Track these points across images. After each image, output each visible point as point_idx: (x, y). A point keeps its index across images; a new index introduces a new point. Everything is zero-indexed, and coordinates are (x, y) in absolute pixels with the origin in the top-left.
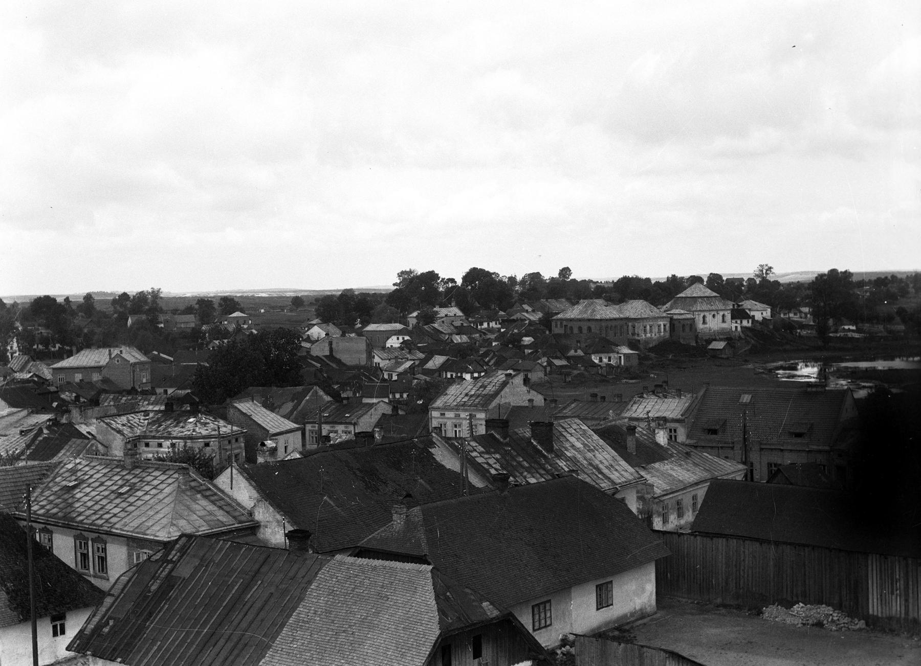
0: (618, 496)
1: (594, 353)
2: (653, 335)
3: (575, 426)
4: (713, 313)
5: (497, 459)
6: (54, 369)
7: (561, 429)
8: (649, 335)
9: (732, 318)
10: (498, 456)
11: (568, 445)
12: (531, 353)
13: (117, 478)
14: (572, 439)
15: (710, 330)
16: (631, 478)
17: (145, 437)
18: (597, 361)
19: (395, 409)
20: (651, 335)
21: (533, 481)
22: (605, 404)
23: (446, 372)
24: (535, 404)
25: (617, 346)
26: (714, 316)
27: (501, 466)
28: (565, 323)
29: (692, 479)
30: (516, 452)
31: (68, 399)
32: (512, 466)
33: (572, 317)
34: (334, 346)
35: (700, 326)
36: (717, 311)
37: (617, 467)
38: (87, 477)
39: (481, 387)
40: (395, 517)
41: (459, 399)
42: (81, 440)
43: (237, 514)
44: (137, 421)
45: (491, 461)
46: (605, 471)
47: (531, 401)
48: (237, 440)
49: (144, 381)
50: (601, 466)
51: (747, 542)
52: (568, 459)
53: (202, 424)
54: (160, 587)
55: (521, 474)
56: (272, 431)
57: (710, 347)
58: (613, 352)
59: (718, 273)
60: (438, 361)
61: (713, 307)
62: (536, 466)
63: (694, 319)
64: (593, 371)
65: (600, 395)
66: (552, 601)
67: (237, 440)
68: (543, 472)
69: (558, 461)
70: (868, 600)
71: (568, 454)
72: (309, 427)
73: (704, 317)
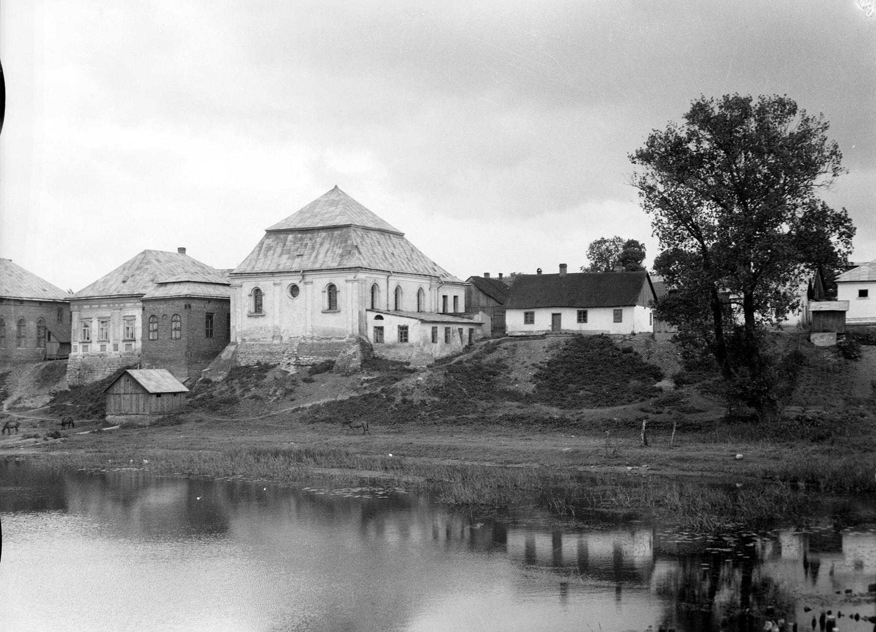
2: (109, 347)
20: (103, 347)
26: (294, 290)
29: (358, 518)
30: (739, 459)
59: (314, 199)
63: (226, 301)
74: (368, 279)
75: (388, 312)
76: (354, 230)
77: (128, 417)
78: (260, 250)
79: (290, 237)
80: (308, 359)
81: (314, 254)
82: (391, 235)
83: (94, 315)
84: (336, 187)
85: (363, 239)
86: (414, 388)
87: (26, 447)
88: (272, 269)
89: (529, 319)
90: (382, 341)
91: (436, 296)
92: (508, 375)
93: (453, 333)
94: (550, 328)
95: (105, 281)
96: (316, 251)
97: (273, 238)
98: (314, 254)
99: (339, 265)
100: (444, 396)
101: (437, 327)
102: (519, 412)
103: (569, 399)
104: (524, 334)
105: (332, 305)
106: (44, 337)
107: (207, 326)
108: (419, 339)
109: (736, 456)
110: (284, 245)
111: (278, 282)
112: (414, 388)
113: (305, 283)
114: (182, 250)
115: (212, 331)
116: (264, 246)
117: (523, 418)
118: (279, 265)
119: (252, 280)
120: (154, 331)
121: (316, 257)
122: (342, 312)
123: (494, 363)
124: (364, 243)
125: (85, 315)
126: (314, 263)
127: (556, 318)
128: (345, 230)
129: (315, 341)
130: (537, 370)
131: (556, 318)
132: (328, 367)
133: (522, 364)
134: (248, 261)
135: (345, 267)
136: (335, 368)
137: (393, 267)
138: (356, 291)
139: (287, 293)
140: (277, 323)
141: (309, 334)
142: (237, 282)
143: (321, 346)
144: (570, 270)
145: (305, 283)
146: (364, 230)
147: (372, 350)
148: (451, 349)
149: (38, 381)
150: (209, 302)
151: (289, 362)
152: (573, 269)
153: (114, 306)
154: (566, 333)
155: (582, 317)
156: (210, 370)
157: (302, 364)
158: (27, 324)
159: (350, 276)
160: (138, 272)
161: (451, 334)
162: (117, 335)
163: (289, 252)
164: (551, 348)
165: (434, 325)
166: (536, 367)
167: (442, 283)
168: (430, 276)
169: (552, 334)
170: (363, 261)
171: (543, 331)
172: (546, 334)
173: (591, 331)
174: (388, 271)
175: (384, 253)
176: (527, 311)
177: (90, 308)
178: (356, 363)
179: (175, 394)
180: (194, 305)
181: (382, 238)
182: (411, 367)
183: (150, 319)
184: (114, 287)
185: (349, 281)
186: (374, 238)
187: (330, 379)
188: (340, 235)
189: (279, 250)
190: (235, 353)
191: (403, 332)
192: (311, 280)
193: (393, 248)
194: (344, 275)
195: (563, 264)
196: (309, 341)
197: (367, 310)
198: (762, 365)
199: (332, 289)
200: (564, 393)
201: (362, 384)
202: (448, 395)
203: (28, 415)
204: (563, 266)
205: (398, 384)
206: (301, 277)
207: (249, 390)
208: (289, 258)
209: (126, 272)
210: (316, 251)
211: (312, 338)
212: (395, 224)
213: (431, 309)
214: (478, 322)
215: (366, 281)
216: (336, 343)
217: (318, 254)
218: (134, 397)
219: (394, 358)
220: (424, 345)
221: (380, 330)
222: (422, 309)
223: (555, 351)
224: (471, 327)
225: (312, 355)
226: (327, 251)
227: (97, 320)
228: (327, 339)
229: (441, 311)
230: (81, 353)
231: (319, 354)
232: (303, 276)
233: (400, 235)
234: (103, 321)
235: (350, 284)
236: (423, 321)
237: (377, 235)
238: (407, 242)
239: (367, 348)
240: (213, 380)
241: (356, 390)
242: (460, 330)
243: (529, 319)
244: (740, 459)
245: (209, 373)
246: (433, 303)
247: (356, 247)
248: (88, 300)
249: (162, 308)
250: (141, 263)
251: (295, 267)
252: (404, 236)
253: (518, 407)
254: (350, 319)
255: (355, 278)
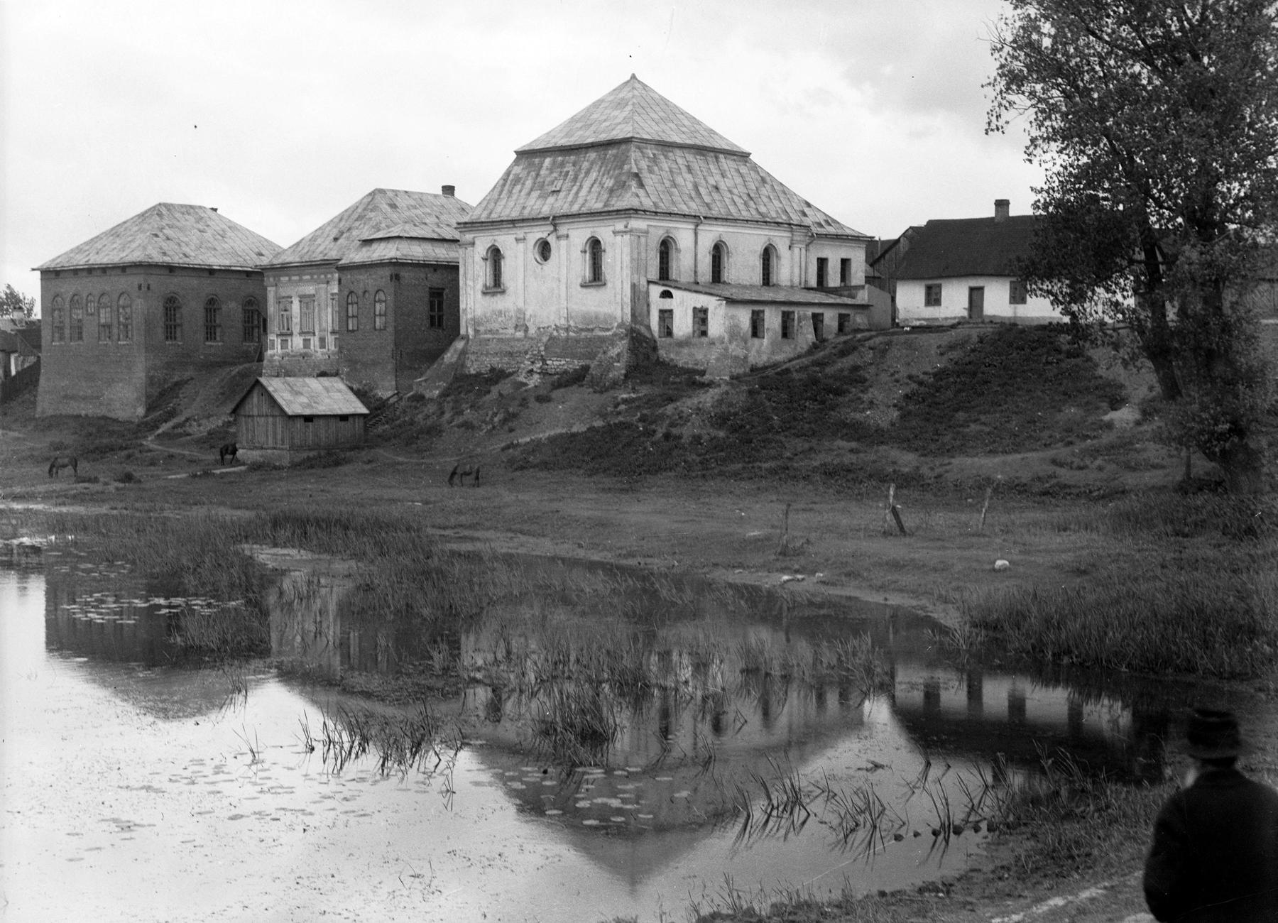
2: (315, 341)
26: (544, 249)
30: (999, 570)
40: (1175, 318)
63: (453, 269)
74: (651, 230)
75: (695, 287)
76: (639, 148)
77: (263, 452)
78: (504, 185)
79: (548, 161)
80: (557, 363)
81: (575, 189)
82: (721, 156)
83: (295, 290)
84: (634, 77)
85: (655, 162)
86: (691, 414)
87: (46, 497)
88: (515, 215)
89: (933, 298)
90: (704, 333)
91: (803, 259)
92: (862, 395)
93: (799, 321)
94: (965, 314)
95: (313, 238)
96: (578, 184)
97: (524, 163)
98: (575, 189)
99: (605, 206)
100: (734, 430)
101: (763, 311)
102: (848, 459)
103: (947, 438)
104: (924, 323)
105: (596, 278)
106: (259, 327)
107: (432, 309)
108: (722, 330)
109: (994, 563)
110: (538, 175)
111: (521, 236)
112: (691, 414)
113: (558, 238)
114: (449, 190)
115: (440, 318)
116: (511, 177)
117: (849, 471)
118: (524, 208)
119: (488, 233)
120: (353, 316)
121: (577, 193)
122: (609, 285)
123: (846, 373)
124: (656, 168)
125: (284, 292)
126: (572, 203)
127: (976, 296)
128: (623, 147)
129: (572, 334)
130: (914, 386)
131: (976, 296)
132: (577, 378)
133: (892, 375)
134: (485, 203)
135: (611, 209)
136: (588, 378)
137: (710, 209)
138: (627, 250)
139: (534, 254)
140: (521, 305)
141: (563, 322)
142: (468, 237)
143: (577, 341)
144: (1014, 211)
145: (558, 238)
146: (660, 148)
147: (655, 349)
148: (795, 348)
149: (223, 394)
150: (435, 270)
151: (530, 368)
152: (1022, 207)
153: (319, 277)
154: (991, 322)
155: (1018, 297)
156: (426, 381)
157: (549, 371)
158: (224, 308)
159: (620, 225)
160: (357, 224)
161: (796, 322)
162: (324, 325)
163: (542, 187)
164: (951, 347)
165: (757, 308)
166: (915, 382)
167: (813, 236)
168: (790, 224)
169: (969, 323)
170: (643, 199)
171: (955, 318)
172: (959, 323)
173: (1032, 319)
174: (695, 216)
175: (696, 187)
176: (930, 282)
177: (290, 280)
178: (619, 369)
179: (344, 418)
180: (405, 274)
181: (697, 162)
182: (707, 378)
183: (347, 299)
184: (321, 249)
185: (619, 232)
186: (680, 161)
187: (575, 396)
188: (615, 156)
189: (529, 183)
190: (463, 352)
191: (701, 316)
192: (565, 232)
193: (718, 178)
194: (611, 222)
195: (1002, 201)
196: (563, 334)
197: (649, 282)
198: (1230, 383)
199: (595, 246)
200: (941, 427)
201: (617, 406)
202: (742, 427)
203: (183, 446)
204: (1002, 205)
205: (670, 409)
206: (551, 228)
207: (461, 413)
208: (540, 197)
209: (341, 225)
210: (578, 184)
211: (567, 330)
212: (733, 134)
213: (791, 281)
214: (863, 303)
215: (647, 232)
216: (599, 337)
217: (581, 187)
218: (270, 419)
219: (687, 363)
220: (730, 342)
221: (666, 315)
222: (775, 281)
223: (955, 355)
224: (843, 311)
225: (564, 357)
226: (592, 185)
227: (298, 299)
228: (588, 330)
229: (813, 282)
230: (280, 351)
231: (573, 356)
232: (555, 225)
233: (744, 157)
234: (306, 300)
235: (619, 238)
236: (731, 301)
237: (687, 155)
238: (755, 168)
239: (644, 345)
240: (427, 396)
241: (603, 416)
242: (817, 319)
243: (933, 298)
244: (1003, 570)
245: (423, 384)
246: (797, 271)
247: (637, 175)
248: (284, 269)
249: (365, 280)
250: (365, 209)
251: (546, 211)
252: (751, 157)
253: (852, 451)
254: (619, 297)
255: (626, 227)
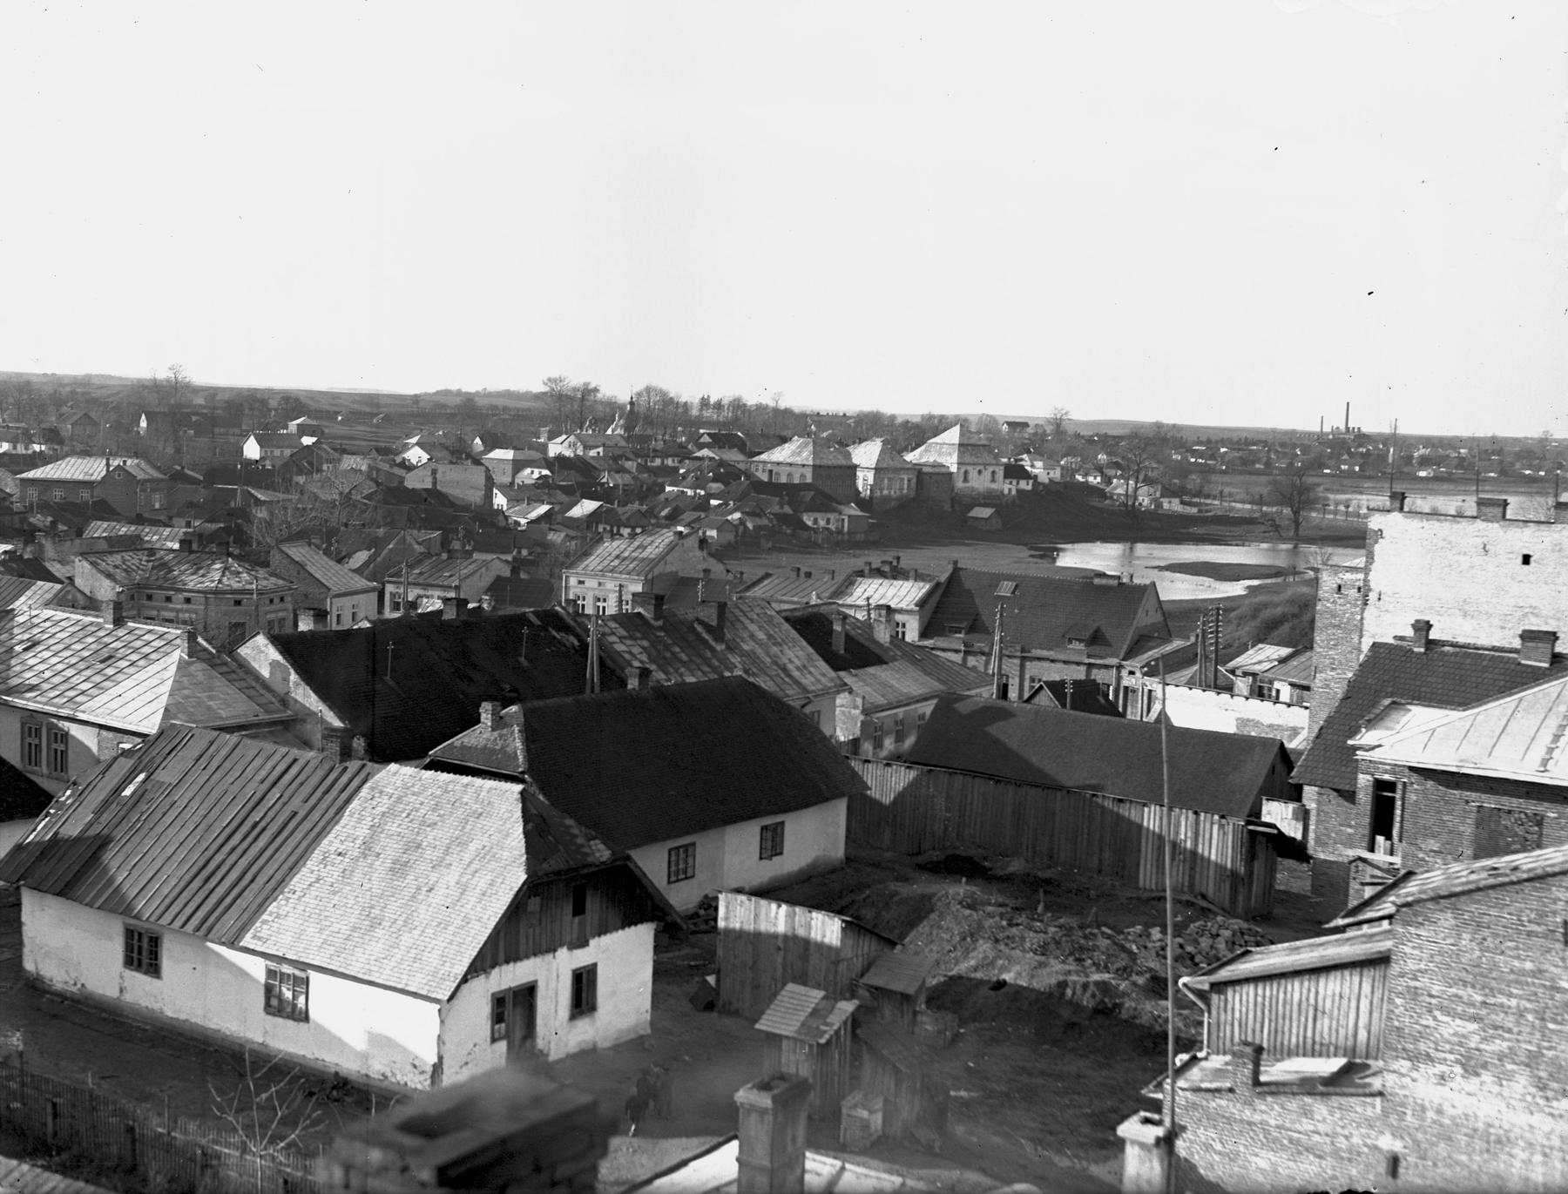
0: (808, 710)
1: (807, 511)
3: (757, 610)
4: (979, 468)
5: (644, 648)
6: (23, 480)
7: (738, 612)
8: (885, 492)
9: (1006, 477)
10: (645, 643)
11: (745, 635)
12: (720, 505)
13: (90, 640)
14: (753, 627)
15: (973, 489)
16: (829, 685)
17: (147, 587)
18: (810, 523)
19: (515, 570)
21: (690, 679)
22: (810, 582)
23: (597, 524)
24: (712, 576)
25: (840, 504)
26: (980, 472)
27: (649, 657)
28: (769, 466)
31: (40, 524)
32: (664, 658)
33: (781, 459)
34: (439, 476)
35: (959, 484)
36: (985, 465)
37: (812, 669)
38: (46, 636)
39: (638, 547)
41: (606, 562)
42: (51, 584)
43: (264, 701)
44: (136, 561)
45: (636, 650)
46: (796, 674)
47: (706, 571)
48: (282, 599)
49: (157, 506)
50: (790, 666)
51: (977, 780)
52: (743, 654)
53: (232, 573)
54: (134, 793)
55: (677, 670)
56: (335, 589)
57: (972, 514)
58: (834, 510)
60: (586, 507)
61: (980, 461)
62: (699, 661)
64: (805, 535)
65: (804, 569)
66: (698, 845)
67: (282, 599)
68: (706, 669)
69: (730, 656)
70: (1138, 865)
71: (746, 647)
72: (389, 588)
73: (966, 472)
